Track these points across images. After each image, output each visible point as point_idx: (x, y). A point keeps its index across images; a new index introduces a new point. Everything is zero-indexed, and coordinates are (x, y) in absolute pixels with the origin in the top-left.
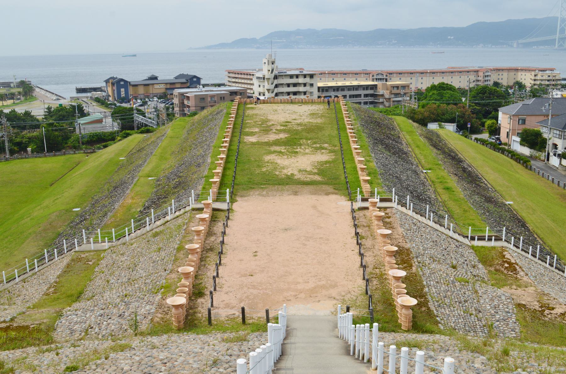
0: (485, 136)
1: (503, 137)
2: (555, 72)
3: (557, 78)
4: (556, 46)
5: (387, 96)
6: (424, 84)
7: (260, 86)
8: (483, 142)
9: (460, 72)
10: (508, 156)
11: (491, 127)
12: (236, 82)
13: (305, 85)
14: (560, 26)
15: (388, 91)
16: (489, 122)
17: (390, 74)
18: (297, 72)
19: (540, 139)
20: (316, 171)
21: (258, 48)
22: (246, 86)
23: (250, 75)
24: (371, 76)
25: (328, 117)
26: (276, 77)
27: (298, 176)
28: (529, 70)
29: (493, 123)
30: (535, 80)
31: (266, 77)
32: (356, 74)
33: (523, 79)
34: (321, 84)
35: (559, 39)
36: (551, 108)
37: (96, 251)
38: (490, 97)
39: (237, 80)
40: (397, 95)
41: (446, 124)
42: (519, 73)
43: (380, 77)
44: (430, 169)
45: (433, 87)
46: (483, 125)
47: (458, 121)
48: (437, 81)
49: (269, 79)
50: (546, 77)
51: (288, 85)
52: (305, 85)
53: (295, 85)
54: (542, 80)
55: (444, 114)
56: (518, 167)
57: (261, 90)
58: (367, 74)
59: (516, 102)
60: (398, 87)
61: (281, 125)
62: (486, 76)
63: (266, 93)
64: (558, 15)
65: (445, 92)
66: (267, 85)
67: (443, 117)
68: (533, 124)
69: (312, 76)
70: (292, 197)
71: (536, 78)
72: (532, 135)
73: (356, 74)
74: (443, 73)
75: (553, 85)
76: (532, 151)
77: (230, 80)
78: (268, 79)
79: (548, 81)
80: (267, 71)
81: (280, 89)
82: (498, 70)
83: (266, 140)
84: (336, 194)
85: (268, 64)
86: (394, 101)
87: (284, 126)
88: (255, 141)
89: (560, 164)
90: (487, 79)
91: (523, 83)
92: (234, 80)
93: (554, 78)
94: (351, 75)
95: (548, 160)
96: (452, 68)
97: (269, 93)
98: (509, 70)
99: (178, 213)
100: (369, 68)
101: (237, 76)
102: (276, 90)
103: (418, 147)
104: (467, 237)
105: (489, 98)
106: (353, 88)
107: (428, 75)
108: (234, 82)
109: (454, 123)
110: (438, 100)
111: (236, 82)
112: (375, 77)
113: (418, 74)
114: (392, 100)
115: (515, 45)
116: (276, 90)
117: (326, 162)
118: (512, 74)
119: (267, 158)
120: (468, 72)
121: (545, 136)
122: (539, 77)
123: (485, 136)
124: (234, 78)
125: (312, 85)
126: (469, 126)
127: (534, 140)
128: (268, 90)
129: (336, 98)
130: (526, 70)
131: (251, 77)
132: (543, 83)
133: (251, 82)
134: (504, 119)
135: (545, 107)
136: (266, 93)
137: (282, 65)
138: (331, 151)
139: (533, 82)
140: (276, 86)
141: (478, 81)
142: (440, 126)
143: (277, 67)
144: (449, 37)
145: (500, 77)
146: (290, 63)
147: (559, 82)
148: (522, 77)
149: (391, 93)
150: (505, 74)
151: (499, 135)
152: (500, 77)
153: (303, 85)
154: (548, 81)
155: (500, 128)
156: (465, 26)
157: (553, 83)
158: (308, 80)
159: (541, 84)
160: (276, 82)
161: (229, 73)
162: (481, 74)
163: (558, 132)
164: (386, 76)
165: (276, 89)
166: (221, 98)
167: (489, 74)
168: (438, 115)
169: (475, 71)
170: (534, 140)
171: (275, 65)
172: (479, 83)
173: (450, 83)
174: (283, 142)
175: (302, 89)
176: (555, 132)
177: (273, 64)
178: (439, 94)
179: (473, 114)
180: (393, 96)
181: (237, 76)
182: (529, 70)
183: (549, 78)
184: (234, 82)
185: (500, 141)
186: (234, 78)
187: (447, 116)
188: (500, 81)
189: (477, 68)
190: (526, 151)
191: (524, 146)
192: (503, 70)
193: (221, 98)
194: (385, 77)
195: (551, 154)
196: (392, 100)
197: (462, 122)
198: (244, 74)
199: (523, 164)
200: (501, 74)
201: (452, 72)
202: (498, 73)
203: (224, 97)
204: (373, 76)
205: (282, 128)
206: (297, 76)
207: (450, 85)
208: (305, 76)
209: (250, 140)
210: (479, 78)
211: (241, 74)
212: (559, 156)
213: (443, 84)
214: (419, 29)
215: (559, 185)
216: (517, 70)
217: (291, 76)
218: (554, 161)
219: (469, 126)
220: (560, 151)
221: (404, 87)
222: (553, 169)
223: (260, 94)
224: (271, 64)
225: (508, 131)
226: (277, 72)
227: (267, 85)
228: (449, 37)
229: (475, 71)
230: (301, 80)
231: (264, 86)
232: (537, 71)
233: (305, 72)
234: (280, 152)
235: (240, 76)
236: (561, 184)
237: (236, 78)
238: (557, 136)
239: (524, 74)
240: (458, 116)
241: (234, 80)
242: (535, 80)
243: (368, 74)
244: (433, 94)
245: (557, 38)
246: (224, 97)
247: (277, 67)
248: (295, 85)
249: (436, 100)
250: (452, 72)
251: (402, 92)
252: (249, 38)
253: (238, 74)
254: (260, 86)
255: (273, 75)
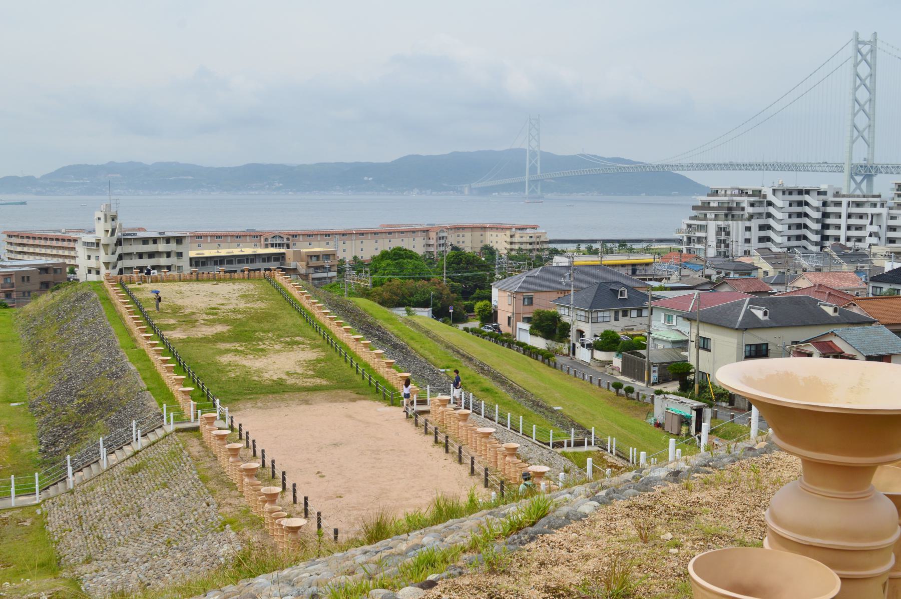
0: (475, 324)
1: (502, 321)
2: (538, 230)
3: (542, 239)
4: (527, 193)
5: (302, 270)
6: (369, 250)
7: (89, 257)
8: (474, 331)
9: (402, 232)
10: (518, 351)
11: (484, 310)
12: (25, 253)
13: (168, 255)
14: (530, 162)
15: (304, 264)
16: (479, 305)
17: (293, 236)
18: (155, 235)
19: (559, 325)
20: (311, 373)
21: (38, 193)
22: (61, 260)
23: (69, 240)
24: (262, 239)
25: (272, 300)
26: (119, 243)
27: (290, 381)
28: (502, 229)
29: (486, 305)
30: (511, 243)
31: (102, 242)
32: (238, 237)
33: (494, 242)
34: (193, 254)
35: (531, 181)
36: (572, 279)
37: (20, 508)
38: (466, 268)
39: (26, 249)
40: (317, 268)
41: (417, 309)
42: (488, 234)
43: (278, 241)
44: (448, 368)
45: (385, 255)
46: (470, 309)
47: (434, 305)
48: (396, 243)
49: (108, 245)
50: (526, 239)
51: (140, 256)
52: (168, 255)
53: (151, 255)
54: (521, 243)
55: (412, 295)
56: (538, 365)
57: (93, 263)
58: (255, 236)
59: (511, 275)
60: (318, 257)
61: (208, 314)
62: (440, 238)
63: (103, 270)
64: (525, 146)
65: (405, 261)
66: (103, 257)
67: (412, 299)
68: (545, 303)
69: (179, 240)
70: (304, 407)
71: (513, 240)
72: (547, 319)
73: (237, 237)
74: (376, 233)
75: (538, 250)
76: (549, 342)
77: (12, 248)
78: (106, 246)
79: (531, 244)
80: (103, 232)
81: (126, 263)
82: (457, 229)
83: (200, 335)
84: (360, 399)
85: (106, 221)
86: (313, 279)
87: (213, 314)
88: (185, 337)
89: (592, 357)
90: (442, 242)
91: (495, 248)
92: (19, 249)
93: (538, 240)
94: (229, 239)
95: (574, 354)
96: (388, 226)
97: (107, 268)
98: (473, 228)
99: (152, 437)
100: (259, 228)
101: (25, 241)
102: (120, 265)
103: (412, 339)
104: (548, 444)
105: (466, 269)
106: (247, 259)
107: (353, 237)
108: (20, 253)
109: (428, 307)
110: (397, 274)
111: (25, 253)
112: (270, 241)
113: (337, 236)
114: (311, 276)
115: (466, 191)
116: (120, 265)
117: (318, 361)
118: (477, 234)
119: (225, 359)
120: (414, 232)
121: (566, 320)
122: (517, 239)
123: (475, 324)
124: (20, 245)
125: (180, 255)
126: (451, 311)
127: (550, 326)
128: (107, 264)
129: (268, 272)
130: (497, 228)
131: (72, 245)
132: (523, 247)
133: (72, 253)
134: (501, 299)
135: (565, 278)
136: (103, 270)
137: (127, 223)
138: (314, 347)
139: (509, 247)
140: (120, 257)
141: (429, 245)
142: (408, 312)
143: (120, 225)
144: (366, 178)
145: (461, 239)
146: (150, 216)
147: (545, 246)
148: (492, 239)
149: (308, 267)
150: (468, 234)
151: (496, 321)
152: (461, 239)
153: (165, 255)
154: (531, 244)
155: (496, 312)
156: (389, 161)
157: (538, 247)
158: (173, 247)
159: (520, 250)
160: (119, 250)
161: (9, 236)
162: (433, 235)
163: (583, 313)
164: (288, 239)
165: (120, 263)
166: (23, 278)
167: (445, 234)
168: (403, 296)
169: (424, 231)
170: (550, 326)
171: (118, 222)
172: (432, 249)
173: (411, 248)
174: (229, 337)
175: (163, 261)
176: (579, 312)
177: (113, 220)
178: (396, 265)
179: (452, 292)
180: (312, 270)
181: (25, 241)
182: (502, 229)
183: (531, 240)
184: (20, 253)
185: (500, 331)
186: (20, 245)
187: (417, 298)
188: (460, 245)
189: (425, 227)
190: (540, 343)
191: (537, 335)
192: (463, 228)
193: (23, 278)
194: (285, 241)
195: (578, 345)
196: (311, 276)
197: (439, 305)
198: (40, 238)
199: (543, 361)
200: (461, 234)
201: (390, 233)
202: (457, 234)
203: (28, 278)
204: (266, 240)
205: (211, 317)
206: (155, 241)
207: (410, 251)
208: (168, 240)
209: (174, 336)
210: (431, 242)
211: (34, 238)
212: (589, 346)
213: (400, 249)
214: (318, 164)
215: (600, 385)
216: (484, 228)
217: (145, 241)
218: (583, 354)
219: (451, 311)
220: (589, 339)
221: (327, 256)
222: (582, 364)
223: (90, 271)
224: (109, 219)
225: (509, 315)
226: (120, 234)
227: (103, 257)
228: (366, 178)
229: (424, 231)
230: (162, 247)
231: (97, 258)
232: (514, 230)
233: (168, 234)
234: (236, 351)
235: (31, 242)
236: (602, 385)
237: (24, 245)
238: (583, 319)
239: (494, 234)
240: (433, 296)
241: (19, 249)
242: (511, 243)
243: (257, 237)
244: (388, 265)
245: (527, 180)
246: (28, 278)
247: (120, 225)
248: (151, 255)
249: (394, 274)
250: (390, 233)
251: (327, 264)
252: (20, 175)
253: (28, 238)
254: (89, 257)
255: (114, 240)
